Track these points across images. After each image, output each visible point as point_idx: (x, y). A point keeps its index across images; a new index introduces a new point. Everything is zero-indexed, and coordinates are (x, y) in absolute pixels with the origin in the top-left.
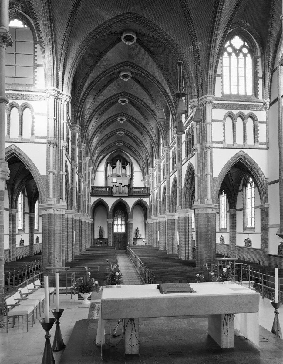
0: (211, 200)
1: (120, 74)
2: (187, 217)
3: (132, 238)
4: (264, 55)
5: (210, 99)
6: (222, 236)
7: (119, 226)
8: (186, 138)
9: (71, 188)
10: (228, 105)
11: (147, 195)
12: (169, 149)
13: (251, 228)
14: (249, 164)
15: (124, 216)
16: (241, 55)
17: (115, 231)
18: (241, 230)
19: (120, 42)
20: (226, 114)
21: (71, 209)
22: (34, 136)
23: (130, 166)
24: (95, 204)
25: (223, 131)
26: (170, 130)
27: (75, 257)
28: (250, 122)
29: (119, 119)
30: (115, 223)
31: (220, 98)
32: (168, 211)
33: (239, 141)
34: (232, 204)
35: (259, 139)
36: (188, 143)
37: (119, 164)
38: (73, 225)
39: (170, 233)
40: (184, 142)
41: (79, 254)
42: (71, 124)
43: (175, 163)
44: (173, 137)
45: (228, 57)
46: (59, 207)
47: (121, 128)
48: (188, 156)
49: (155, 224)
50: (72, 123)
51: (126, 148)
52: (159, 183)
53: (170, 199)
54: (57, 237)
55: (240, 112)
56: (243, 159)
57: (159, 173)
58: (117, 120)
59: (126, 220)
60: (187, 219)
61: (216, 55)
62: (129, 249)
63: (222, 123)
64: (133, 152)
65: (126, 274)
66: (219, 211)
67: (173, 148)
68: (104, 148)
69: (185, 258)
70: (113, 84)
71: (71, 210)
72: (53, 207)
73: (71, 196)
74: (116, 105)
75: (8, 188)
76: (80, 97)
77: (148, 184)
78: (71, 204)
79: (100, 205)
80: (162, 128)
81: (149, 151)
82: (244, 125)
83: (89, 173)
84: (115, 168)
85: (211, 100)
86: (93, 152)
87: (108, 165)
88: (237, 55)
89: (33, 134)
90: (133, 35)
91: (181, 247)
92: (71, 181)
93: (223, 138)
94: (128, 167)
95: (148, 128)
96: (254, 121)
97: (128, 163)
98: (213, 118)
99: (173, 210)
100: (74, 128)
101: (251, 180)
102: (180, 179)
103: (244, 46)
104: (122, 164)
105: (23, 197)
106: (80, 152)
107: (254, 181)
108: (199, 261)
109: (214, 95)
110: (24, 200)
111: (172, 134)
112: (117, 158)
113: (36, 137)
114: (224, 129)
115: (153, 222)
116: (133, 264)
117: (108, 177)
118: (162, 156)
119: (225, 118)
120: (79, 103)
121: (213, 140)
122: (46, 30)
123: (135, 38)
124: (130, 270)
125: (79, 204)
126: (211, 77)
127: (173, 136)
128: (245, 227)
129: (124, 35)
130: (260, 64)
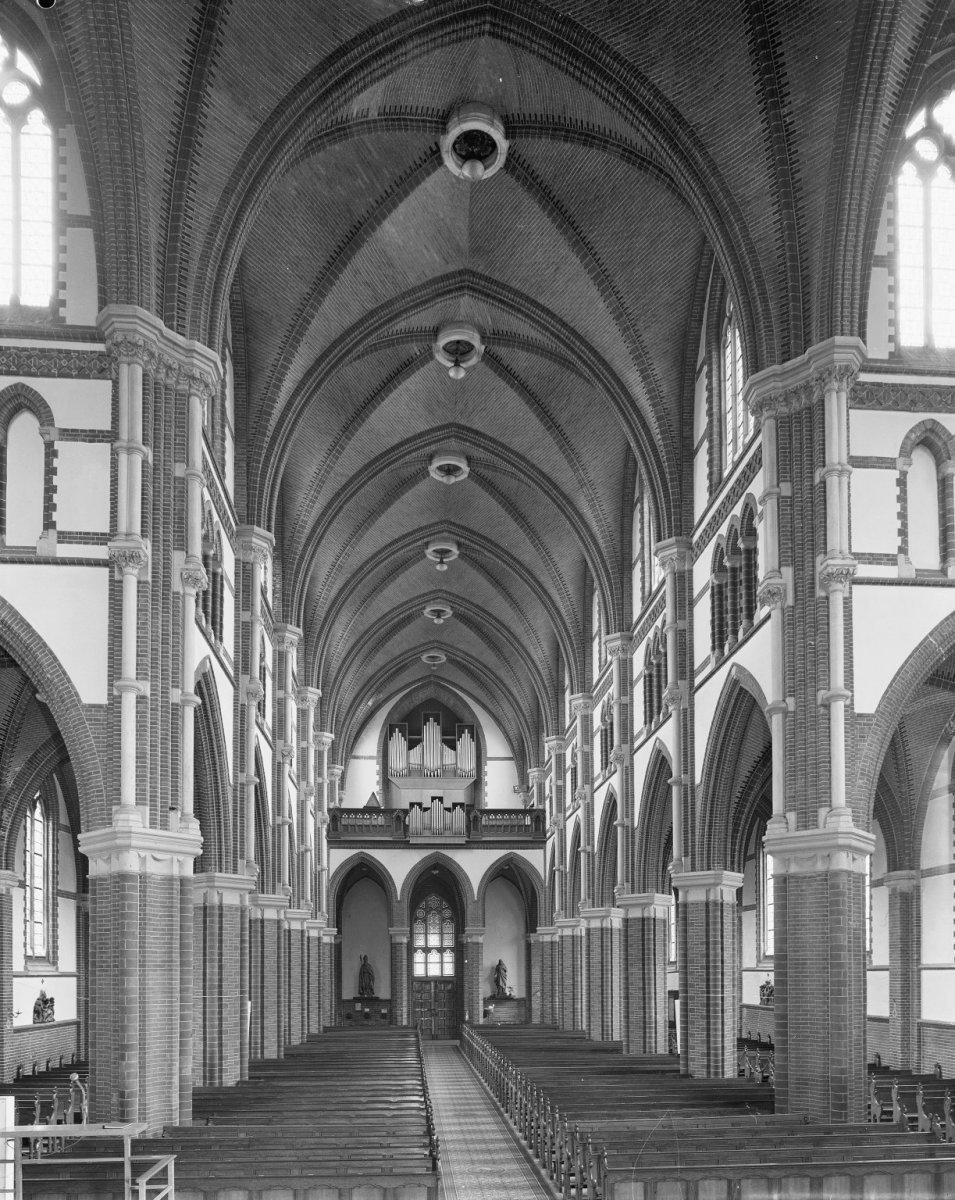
1: (436, 340)
2: (715, 904)
3: (481, 997)
5: (843, 356)
7: (434, 957)
8: (714, 571)
9: (236, 783)
11: (539, 842)
12: (630, 642)
15: (451, 918)
17: (419, 971)
20: (911, 431)
21: (235, 871)
22: (53, 534)
23: (472, 737)
24: (344, 872)
25: (898, 507)
26: (596, 641)
27: (251, 1068)
29: (428, 609)
30: (420, 942)
31: (882, 361)
37: (432, 732)
38: (242, 935)
39: (635, 971)
40: (701, 595)
41: (275, 1056)
42: (236, 524)
43: (612, 745)
44: (647, 594)
45: (919, 182)
47: (440, 591)
48: (722, 647)
49: (568, 944)
50: (240, 521)
52: (587, 787)
53: (637, 840)
54: (155, 979)
57: (586, 748)
58: (425, 556)
59: (459, 930)
60: (715, 911)
62: (469, 1034)
63: (896, 474)
64: (483, 685)
65: (464, 1147)
66: (758, 899)
67: (605, 698)
68: (377, 668)
69: (709, 1073)
70: (408, 390)
71: (233, 876)
73: (235, 816)
74: (422, 487)
76: (270, 414)
77: (542, 798)
78: (235, 852)
79: (361, 877)
80: (603, 561)
81: (544, 672)
83: (332, 784)
84: (418, 749)
86: (336, 678)
87: (391, 735)
89: (49, 524)
90: (460, 465)
91: (690, 1026)
92: (235, 756)
93: (898, 541)
94: (465, 743)
95: (542, 579)
97: (467, 727)
100: (247, 539)
104: (444, 733)
105: (51, 832)
106: (303, 714)
108: (792, 1087)
110: (56, 840)
111: (643, 583)
112: (430, 712)
113: (65, 537)
114: (902, 498)
115: (562, 937)
116: (487, 1093)
117: (393, 779)
118: (599, 681)
119: (906, 452)
120: (267, 439)
122: (96, 28)
123: (503, 145)
124: (479, 1120)
125: (274, 859)
126: (850, 255)
127: (647, 589)
129: (455, 132)
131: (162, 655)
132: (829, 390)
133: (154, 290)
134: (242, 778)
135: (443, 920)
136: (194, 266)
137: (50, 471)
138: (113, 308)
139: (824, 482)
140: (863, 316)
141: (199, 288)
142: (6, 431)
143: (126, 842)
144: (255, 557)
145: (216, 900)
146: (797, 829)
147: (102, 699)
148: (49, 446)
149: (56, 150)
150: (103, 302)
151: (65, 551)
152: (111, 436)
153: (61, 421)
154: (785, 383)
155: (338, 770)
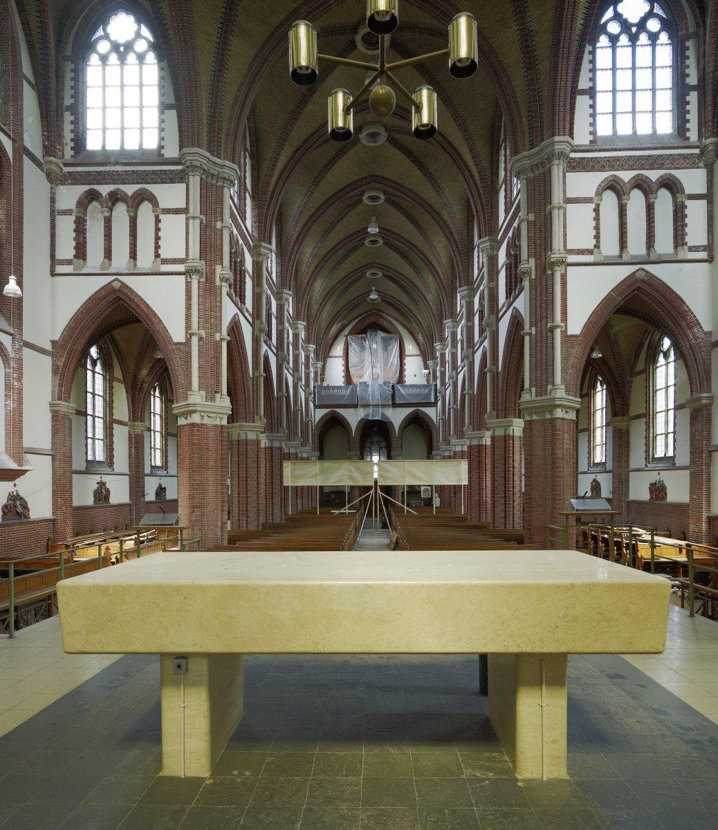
0: (563, 386)
4: (705, 30)
5: (559, 147)
6: (594, 480)
8: (506, 256)
10: (609, 160)
13: (665, 459)
14: (662, 299)
15: (385, 447)
16: (643, 38)
18: (642, 464)
19: (353, 51)
22: (159, 260)
24: (323, 421)
25: (594, 224)
28: (664, 201)
31: (585, 146)
32: (471, 427)
33: (637, 246)
34: (618, 407)
35: (687, 239)
36: (511, 268)
46: (213, 410)
47: (373, 263)
51: (389, 307)
53: (476, 402)
55: (638, 175)
56: (647, 288)
57: (454, 350)
58: (364, 244)
61: (577, 38)
63: (593, 206)
64: (402, 314)
71: (253, 424)
72: (198, 409)
74: (360, 207)
75: (124, 377)
81: (433, 307)
82: (650, 209)
85: (564, 149)
88: (634, 39)
89: (157, 255)
93: (594, 242)
95: (428, 256)
96: (674, 194)
98: (571, 194)
99: (479, 425)
101: (667, 343)
102: (494, 352)
103: (650, 14)
107: (676, 345)
109: (573, 138)
113: (165, 261)
114: (597, 219)
119: (599, 193)
120: (268, 197)
121: (568, 248)
122: (177, 20)
125: (278, 415)
128: (651, 457)
130: (691, 53)
131: (211, 312)
132: (553, 165)
133: (205, 138)
134: (257, 374)
135: (381, 448)
136: (225, 124)
137: (158, 230)
138: (186, 150)
139: (551, 213)
140: (572, 124)
141: (227, 134)
142: (137, 211)
143: (194, 408)
144: (263, 259)
145: (243, 437)
146: (536, 396)
147: (183, 340)
148: (157, 217)
149: (160, 73)
150: (181, 147)
151: (165, 268)
152: (185, 211)
153: (163, 205)
154: (531, 161)
155: (320, 364)
